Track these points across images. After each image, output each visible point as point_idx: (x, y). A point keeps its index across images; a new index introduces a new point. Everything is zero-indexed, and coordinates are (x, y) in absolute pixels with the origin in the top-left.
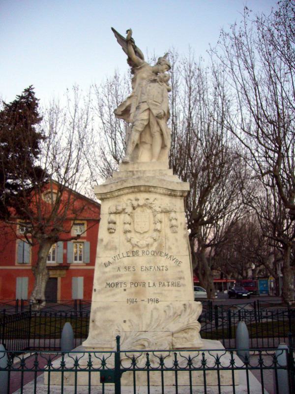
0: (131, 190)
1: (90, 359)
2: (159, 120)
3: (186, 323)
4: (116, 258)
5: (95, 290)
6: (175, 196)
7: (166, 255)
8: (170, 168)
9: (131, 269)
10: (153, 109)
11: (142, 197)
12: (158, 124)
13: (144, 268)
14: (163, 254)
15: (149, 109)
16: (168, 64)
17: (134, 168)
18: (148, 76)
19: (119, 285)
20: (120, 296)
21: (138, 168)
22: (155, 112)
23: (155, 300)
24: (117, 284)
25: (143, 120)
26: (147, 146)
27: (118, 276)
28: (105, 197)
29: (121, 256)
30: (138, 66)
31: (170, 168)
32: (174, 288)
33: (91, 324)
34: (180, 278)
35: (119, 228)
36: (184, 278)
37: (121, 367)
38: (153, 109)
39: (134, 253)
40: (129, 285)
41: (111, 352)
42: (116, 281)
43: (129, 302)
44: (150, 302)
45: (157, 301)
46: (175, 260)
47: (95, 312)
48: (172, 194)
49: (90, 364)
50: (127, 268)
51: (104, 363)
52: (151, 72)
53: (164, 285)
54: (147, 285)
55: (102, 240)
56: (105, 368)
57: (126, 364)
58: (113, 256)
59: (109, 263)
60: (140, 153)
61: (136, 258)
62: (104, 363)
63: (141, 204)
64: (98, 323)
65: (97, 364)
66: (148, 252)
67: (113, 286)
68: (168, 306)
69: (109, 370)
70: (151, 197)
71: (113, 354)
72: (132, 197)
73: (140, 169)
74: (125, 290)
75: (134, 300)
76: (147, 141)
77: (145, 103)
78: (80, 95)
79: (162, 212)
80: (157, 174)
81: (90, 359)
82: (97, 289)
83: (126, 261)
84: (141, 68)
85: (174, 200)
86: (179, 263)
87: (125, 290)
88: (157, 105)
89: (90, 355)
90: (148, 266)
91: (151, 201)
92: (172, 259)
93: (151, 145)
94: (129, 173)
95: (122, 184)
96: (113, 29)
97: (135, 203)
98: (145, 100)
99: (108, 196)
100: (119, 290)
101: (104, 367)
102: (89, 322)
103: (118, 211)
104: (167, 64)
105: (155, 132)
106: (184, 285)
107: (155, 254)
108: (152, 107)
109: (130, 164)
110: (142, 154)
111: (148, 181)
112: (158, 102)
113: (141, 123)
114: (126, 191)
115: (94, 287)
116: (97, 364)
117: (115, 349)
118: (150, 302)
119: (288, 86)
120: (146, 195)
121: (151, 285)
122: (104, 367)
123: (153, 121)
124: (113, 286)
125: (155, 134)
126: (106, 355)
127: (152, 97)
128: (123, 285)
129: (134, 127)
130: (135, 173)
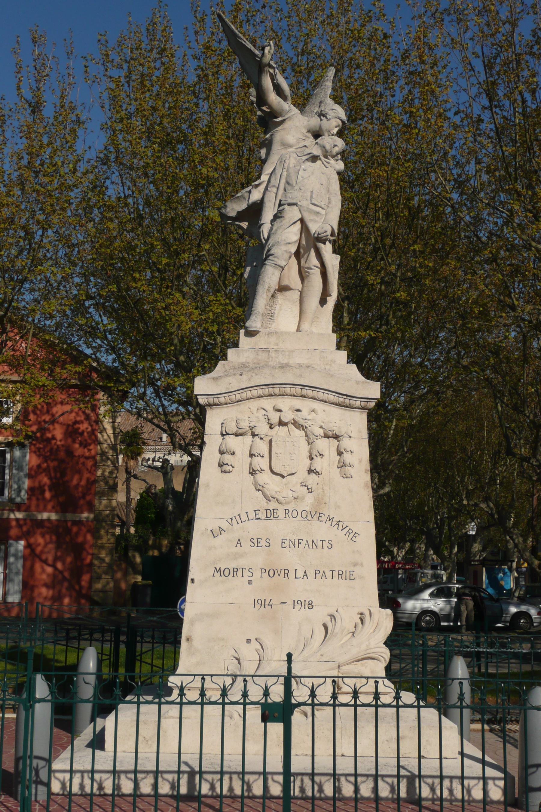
0: (266, 391)
1: (245, 686)
2: (321, 245)
3: (364, 647)
4: (234, 520)
5: (193, 580)
6: (350, 407)
7: (330, 519)
8: (338, 348)
9: (263, 543)
11: (286, 404)
13: (287, 543)
14: (324, 518)
15: (302, 220)
17: (269, 343)
18: (298, 141)
19: (240, 573)
20: (239, 591)
23: (307, 602)
24: (235, 571)
27: (236, 556)
28: (216, 401)
29: (244, 517)
30: (276, 118)
31: (338, 348)
32: (342, 582)
33: (184, 645)
34: (355, 565)
35: (241, 462)
36: (362, 565)
37: (293, 701)
39: (270, 514)
40: (257, 574)
41: (278, 676)
42: (232, 565)
43: (258, 606)
44: (298, 607)
45: (310, 605)
46: (347, 529)
47: (192, 623)
48: (345, 402)
49: (245, 695)
50: (255, 541)
51: (266, 693)
52: (305, 131)
53: (324, 575)
54: (292, 575)
55: (208, 486)
56: (269, 701)
57: (300, 694)
58: (228, 517)
59: (221, 530)
60: (278, 307)
61: (272, 523)
62: (266, 693)
63: (285, 420)
64: (196, 643)
65: (256, 694)
66: (295, 512)
67: (227, 571)
68: (331, 615)
69: (275, 704)
70: (305, 405)
71: (282, 680)
72: (268, 404)
73: (281, 345)
74: (250, 582)
75: (267, 603)
77: (295, 207)
79: (326, 436)
81: (245, 686)
82: (195, 580)
83: (253, 528)
84: (283, 122)
85: (348, 414)
86: (353, 535)
87: (250, 582)
88: (318, 213)
89: (245, 680)
90: (295, 538)
91: (305, 413)
92: (340, 528)
94: (260, 353)
95: (250, 379)
97: (275, 417)
99: (222, 400)
100: (238, 581)
101: (266, 700)
102: (179, 642)
103: (240, 431)
106: (361, 577)
107: (309, 517)
108: (308, 217)
110: (280, 309)
114: (255, 393)
115: (191, 576)
116: (256, 694)
117: (285, 672)
118: (298, 607)
119: (535, 344)
120: (297, 403)
121: (300, 574)
122: (266, 700)
124: (227, 571)
126: (271, 681)
127: (309, 194)
128: (246, 573)
129: (271, 258)
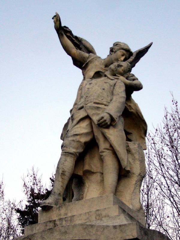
2: (106, 131)
10: (94, 114)
12: (106, 138)
16: (125, 47)
21: (66, 214)
22: (95, 119)
25: (77, 135)
26: (96, 178)
38: (94, 114)
76: (94, 169)
78: (77, 128)
80: (93, 218)
88: (98, 108)
93: (58, 168)
96: (62, 31)
98: (81, 105)
104: (123, 49)
105: (103, 152)
108: (91, 112)
109: (54, 209)
110: (88, 191)
111: (75, 238)
112: (102, 104)
113: (73, 140)
123: (98, 134)
125: (104, 154)
130: (58, 223)
